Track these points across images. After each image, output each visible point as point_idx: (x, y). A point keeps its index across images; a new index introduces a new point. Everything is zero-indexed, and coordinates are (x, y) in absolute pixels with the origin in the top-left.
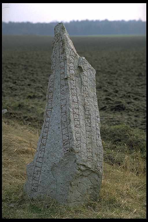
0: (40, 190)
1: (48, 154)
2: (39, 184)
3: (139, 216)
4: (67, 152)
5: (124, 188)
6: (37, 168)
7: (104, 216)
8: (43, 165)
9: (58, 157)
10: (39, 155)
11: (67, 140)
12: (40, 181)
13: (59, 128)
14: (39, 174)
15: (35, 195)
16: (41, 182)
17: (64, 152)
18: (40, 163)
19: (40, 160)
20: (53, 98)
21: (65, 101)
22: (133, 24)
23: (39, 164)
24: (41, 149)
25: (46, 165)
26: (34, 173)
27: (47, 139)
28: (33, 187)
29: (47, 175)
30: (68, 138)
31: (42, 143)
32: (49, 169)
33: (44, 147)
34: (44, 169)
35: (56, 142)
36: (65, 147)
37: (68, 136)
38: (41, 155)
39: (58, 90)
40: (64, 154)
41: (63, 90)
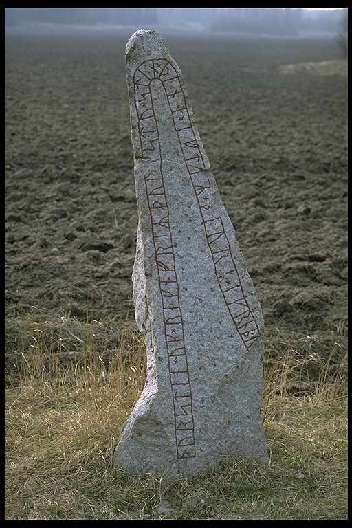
0: (202, 448)
1: (199, 359)
2: (195, 436)
3: (330, 516)
4: (252, 341)
5: (310, 424)
6: (178, 399)
7: (282, 514)
8: (192, 389)
9: (230, 358)
10: (172, 367)
11: (246, 314)
12: (196, 428)
13: (212, 290)
14: (189, 413)
15: (195, 466)
16: (200, 430)
17: (244, 342)
18: (184, 384)
19: (182, 378)
20: (170, 221)
21: (219, 224)
22: (314, 50)
23: (183, 390)
24: (173, 352)
25: (200, 386)
26: (176, 415)
27: (182, 322)
28: (183, 449)
29: (213, 407)
30: (247, 308)
31: (166, 336)
32: (213, 394)
33: (179, 345)
34: (198, 397)
35: (215, 325)
36: (242, 330)
37: (247, 305)
38: (181, 366)
39: (188, 200)
40: (245, 349)
41: (206, 199)
